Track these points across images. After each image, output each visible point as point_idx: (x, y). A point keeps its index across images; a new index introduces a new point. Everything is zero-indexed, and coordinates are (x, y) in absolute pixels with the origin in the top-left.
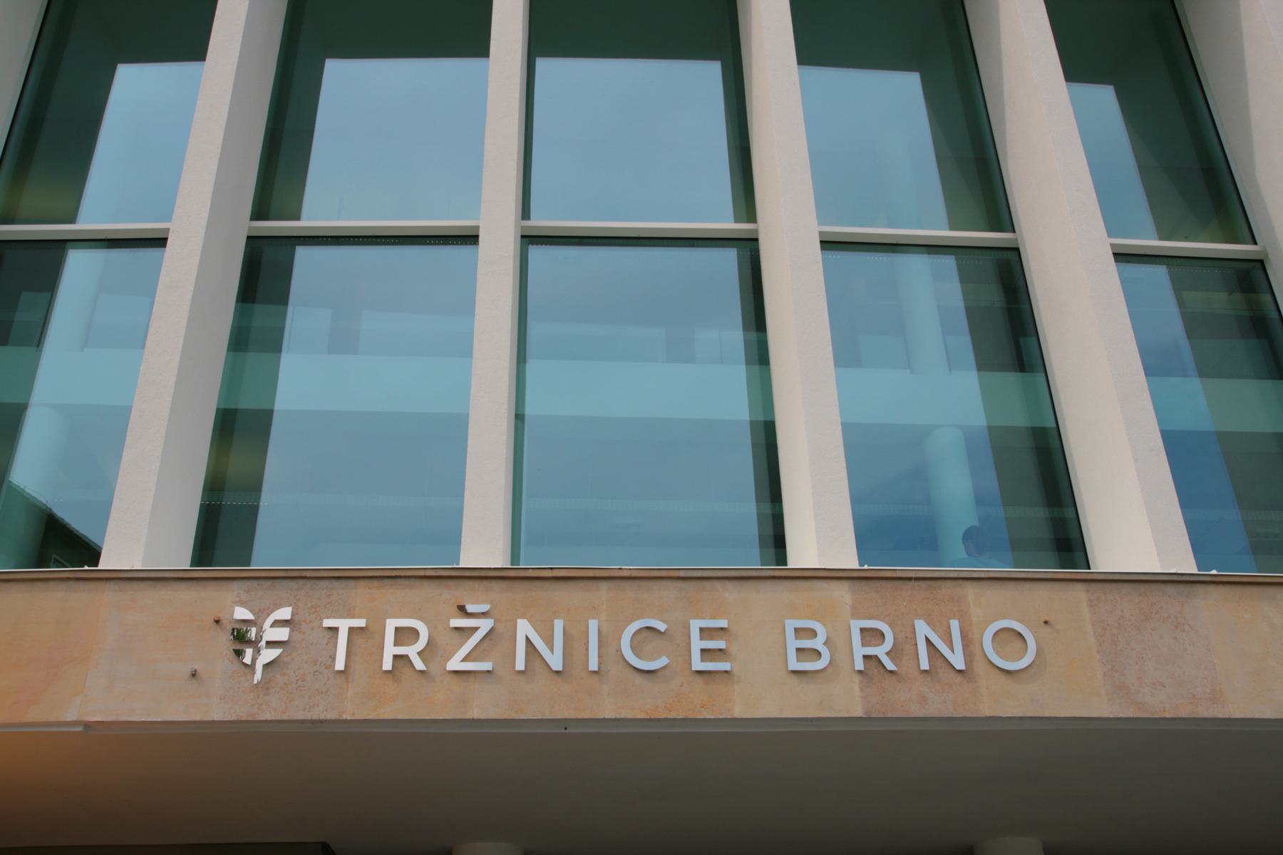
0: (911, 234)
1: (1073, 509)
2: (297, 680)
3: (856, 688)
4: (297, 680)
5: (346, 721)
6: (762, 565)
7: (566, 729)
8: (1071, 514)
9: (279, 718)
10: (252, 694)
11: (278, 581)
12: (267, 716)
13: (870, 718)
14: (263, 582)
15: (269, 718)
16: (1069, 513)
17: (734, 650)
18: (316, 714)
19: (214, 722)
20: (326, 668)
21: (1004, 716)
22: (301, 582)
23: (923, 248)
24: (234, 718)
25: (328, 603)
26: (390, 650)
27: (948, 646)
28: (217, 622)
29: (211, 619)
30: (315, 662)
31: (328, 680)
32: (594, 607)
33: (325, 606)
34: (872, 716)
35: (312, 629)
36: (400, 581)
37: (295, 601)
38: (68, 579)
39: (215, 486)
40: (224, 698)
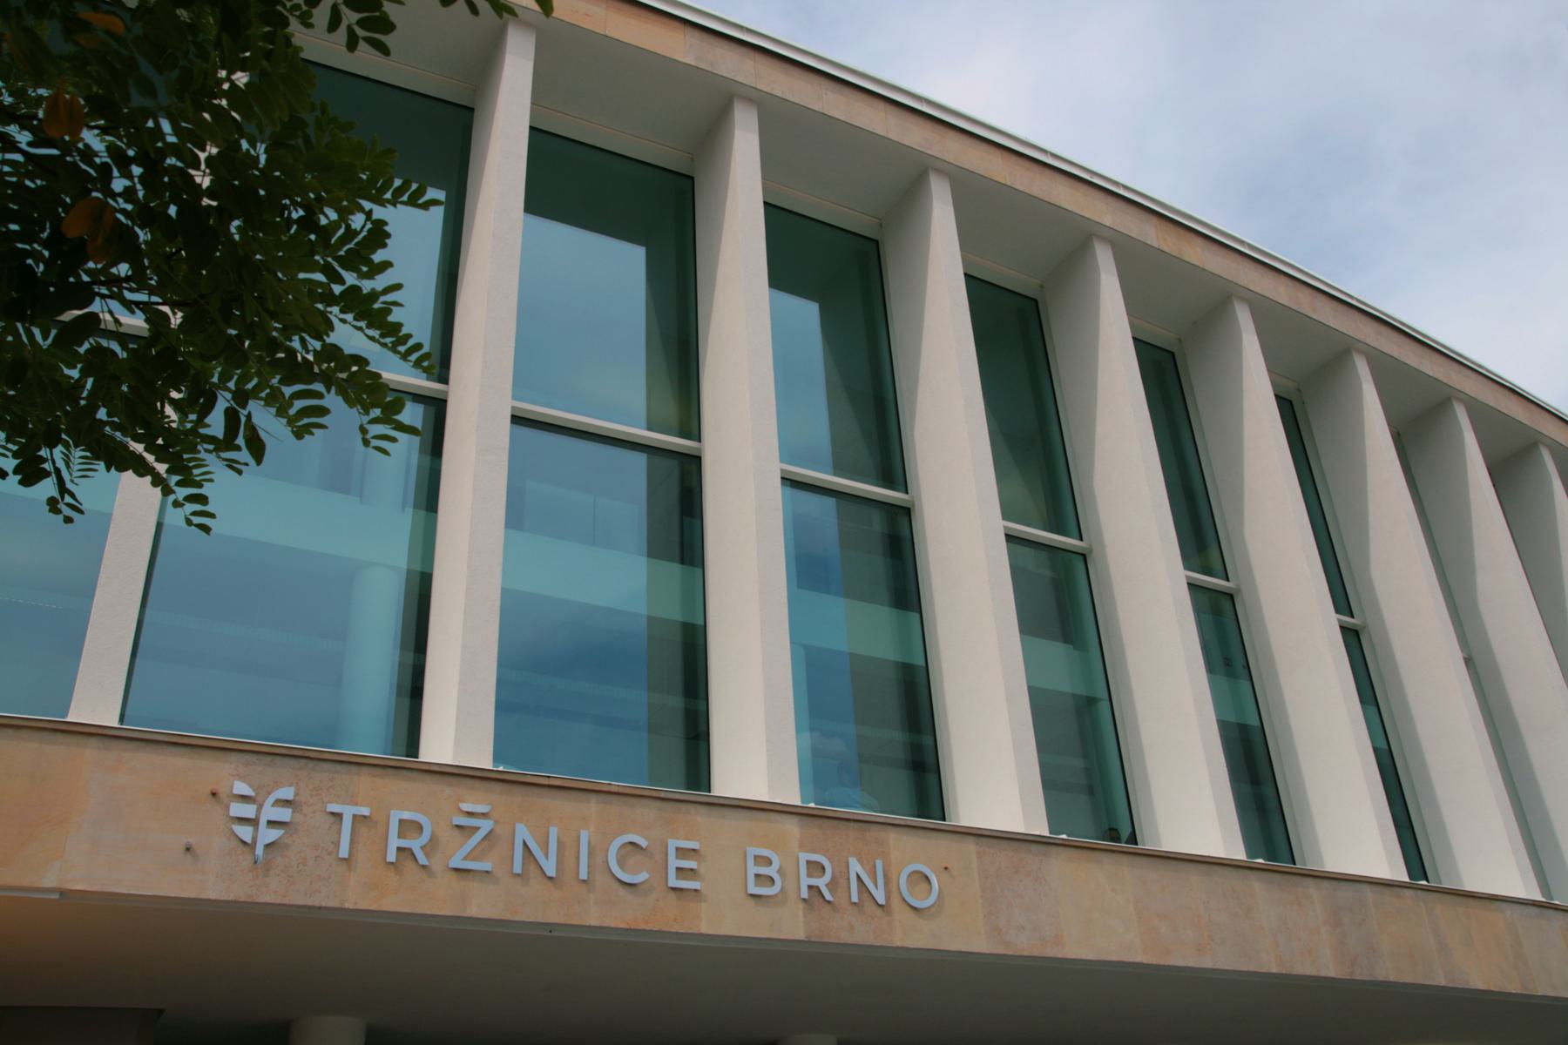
3: (801, 913)
12: (267, 898)
22: (303, 762)
26: (394, 842)
28: (214, 794)
29: (208, 791)
30: (317, 847)
35: (314, 812)
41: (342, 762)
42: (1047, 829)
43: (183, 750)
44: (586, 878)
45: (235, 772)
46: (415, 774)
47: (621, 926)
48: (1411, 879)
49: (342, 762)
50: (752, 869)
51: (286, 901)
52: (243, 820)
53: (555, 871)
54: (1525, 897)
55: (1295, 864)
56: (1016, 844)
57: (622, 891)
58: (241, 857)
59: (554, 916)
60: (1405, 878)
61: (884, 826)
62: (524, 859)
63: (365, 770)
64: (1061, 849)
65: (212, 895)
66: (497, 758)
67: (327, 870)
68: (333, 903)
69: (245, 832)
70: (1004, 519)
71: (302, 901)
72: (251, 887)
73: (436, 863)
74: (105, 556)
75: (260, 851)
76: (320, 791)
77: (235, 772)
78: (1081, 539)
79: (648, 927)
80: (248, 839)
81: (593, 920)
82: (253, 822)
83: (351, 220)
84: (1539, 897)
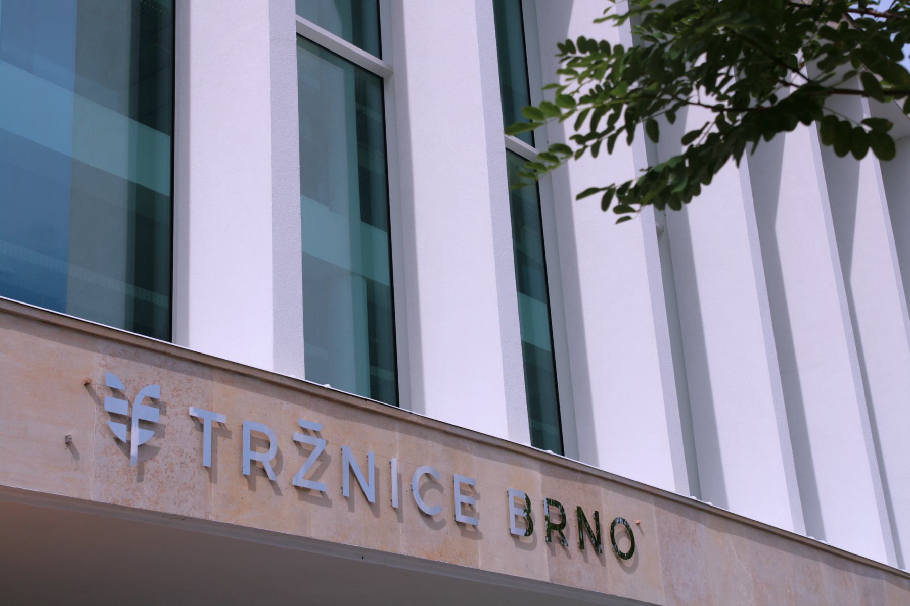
0: (354, 50)
1: (166, 299)
2: (167, 469)
3: (545, 555)
4: (167, 469)
5: (210, 522)
6: (371, 398)
7: (363, 558)
8: (161, 300)
9: (152, 508)
10: (126, 477)
11: (141, 351)
12: (140, 504)
13: (552, 584)
14: (127, 349)
15: (144, 508)
16: (160, 300)
17: (477, 506)
18: (184, 510)
19: (90, 502)
20: (191, 461)
21: (618, 596)
22: (163, 358)
23: (317, 48)
24: (110, 501)
25: (188, 389)
26: (248, 455)
27: (628, 537)
28: (87, 384)
29: (83, 378)
30: (181, 452)
31: (194, 474)
32: (391, 446)
33: (186, 391)
34: (554, 583)
35: (176, 414)
36: (249, 381)
37: (159, 379)
38: (107, 339)
39: (529, 351)
40: (99, 477)
41: (196, 363)
42: (303, 373)
43: (54, 330)
44: (209, 465)
45: (103, 362)
46: (258, 383)
47: (423, 557)
48: (534, 444)
49: (196, 363)
50: (460, 498)
51: (158, 508)
52: (115, 416)
53: (397, 504)
54: (793, 531)
55: (563, 454)
56: (680, 507)
57: (421, 522)
58: (115, 457)
59: (374, 543)
60: (526, 440)
61: (597, 479)
62: (350, 482)
63: (217, 374)
64: (707, 515)
65: (93, 498)
66: (307, 375)
67: (192, 478)
68: (198, 514)
69: (119, 429)
70: (298, 12)
71: (172, 509)
72: (127, 490)
73: (281, 481)
74: (874, 450)
75: (134, 451)
76: (180, 393)
77: (103, 362)
78: (381, 58)
79: (442, 560)
80: (124, 439)
81: (403, 550)
82: (127, 420)
83: (713, 95)
84: (686, 493)
